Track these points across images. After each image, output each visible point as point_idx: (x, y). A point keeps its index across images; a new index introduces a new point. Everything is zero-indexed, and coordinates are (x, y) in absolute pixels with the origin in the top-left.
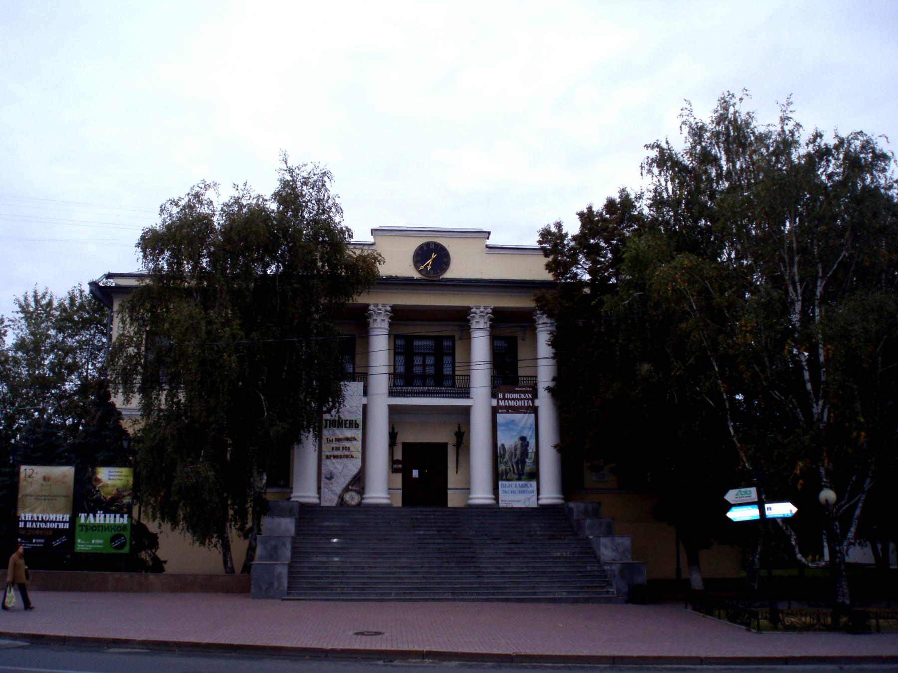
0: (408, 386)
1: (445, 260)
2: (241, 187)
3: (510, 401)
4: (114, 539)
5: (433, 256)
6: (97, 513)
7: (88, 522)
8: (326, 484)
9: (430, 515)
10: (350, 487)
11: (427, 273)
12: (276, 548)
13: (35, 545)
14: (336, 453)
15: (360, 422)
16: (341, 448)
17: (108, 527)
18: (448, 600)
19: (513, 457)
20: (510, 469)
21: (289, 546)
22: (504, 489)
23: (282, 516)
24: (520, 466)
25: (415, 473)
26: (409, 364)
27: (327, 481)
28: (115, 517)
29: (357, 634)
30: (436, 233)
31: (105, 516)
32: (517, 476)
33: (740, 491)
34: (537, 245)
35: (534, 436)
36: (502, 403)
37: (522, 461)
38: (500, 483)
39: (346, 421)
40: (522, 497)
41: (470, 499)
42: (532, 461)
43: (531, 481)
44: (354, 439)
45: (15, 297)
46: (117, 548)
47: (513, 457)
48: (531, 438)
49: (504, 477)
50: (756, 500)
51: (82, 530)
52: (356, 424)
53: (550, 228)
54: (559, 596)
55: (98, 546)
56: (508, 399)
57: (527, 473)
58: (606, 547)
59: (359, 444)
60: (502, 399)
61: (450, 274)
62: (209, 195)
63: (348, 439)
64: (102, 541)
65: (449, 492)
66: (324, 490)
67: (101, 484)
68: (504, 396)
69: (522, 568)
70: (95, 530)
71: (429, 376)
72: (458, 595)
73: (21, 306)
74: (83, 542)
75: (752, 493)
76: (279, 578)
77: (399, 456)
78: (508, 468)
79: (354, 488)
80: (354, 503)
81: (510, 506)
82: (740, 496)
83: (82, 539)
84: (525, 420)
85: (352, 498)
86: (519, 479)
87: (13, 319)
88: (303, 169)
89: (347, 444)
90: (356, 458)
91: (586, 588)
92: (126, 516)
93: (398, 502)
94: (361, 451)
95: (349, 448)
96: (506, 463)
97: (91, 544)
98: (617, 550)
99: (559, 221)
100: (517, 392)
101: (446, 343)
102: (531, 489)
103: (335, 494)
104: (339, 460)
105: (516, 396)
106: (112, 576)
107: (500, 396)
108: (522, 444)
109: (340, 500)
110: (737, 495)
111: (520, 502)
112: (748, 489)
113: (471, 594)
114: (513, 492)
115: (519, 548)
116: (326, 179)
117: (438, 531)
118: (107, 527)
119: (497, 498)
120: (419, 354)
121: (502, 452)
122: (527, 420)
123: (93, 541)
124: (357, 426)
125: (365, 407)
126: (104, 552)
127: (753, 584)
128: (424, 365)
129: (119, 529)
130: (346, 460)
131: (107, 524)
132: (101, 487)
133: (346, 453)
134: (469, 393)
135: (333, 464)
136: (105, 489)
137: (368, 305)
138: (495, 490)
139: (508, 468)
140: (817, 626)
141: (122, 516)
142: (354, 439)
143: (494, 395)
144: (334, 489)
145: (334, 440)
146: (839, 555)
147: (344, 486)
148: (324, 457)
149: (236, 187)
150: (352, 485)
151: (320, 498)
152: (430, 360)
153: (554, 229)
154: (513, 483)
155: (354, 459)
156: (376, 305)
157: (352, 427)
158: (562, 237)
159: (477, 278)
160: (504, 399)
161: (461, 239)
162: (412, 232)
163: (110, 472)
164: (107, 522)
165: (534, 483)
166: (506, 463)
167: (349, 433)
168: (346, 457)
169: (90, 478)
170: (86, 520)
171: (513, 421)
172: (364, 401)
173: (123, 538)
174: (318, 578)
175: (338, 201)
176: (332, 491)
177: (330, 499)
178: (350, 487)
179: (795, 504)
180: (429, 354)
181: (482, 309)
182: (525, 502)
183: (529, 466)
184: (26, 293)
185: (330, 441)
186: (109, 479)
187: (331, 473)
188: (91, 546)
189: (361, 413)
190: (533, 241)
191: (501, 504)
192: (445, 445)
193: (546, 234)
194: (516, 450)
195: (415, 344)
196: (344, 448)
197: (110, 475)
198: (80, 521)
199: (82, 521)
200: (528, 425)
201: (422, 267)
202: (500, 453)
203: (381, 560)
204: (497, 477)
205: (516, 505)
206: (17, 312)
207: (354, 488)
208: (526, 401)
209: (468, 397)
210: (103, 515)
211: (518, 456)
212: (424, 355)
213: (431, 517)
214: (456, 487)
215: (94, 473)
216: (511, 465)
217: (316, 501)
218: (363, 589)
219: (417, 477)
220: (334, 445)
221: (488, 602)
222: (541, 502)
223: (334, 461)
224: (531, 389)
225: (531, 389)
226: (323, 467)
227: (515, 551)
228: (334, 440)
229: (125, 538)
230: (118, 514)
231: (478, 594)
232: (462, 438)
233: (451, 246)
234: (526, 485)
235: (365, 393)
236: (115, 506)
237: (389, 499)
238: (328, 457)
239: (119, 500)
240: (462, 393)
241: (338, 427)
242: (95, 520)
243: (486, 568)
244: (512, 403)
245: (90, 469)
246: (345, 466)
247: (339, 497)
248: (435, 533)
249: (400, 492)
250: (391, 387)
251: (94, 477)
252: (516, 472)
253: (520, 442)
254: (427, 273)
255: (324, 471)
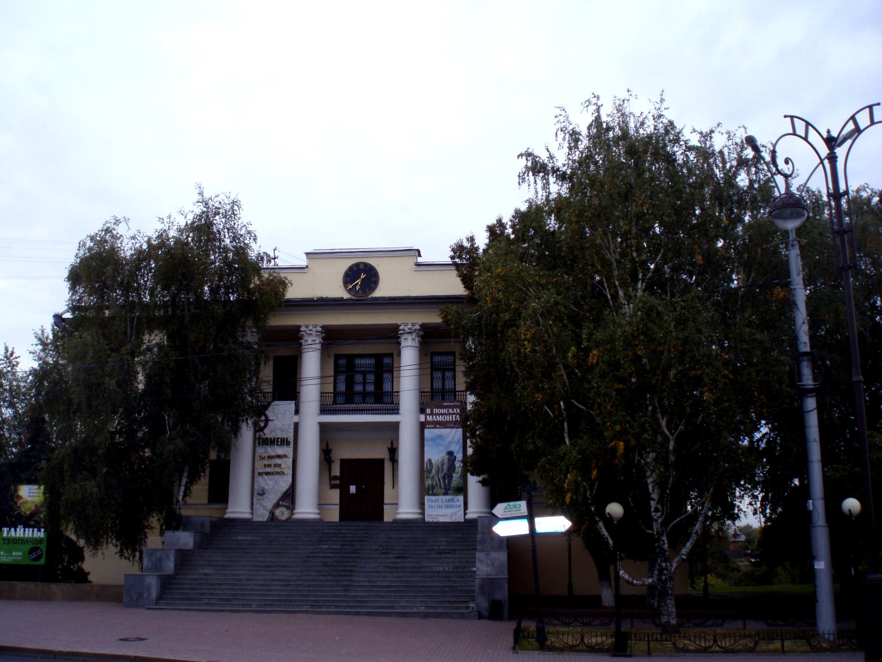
0: (380, 404)
1: (373, 279)
2: (166, 220)
3: (438, 416)
4: (32, 551)
5: (363, 276)
6: (17, 527)
7: (9, 536)
8: (258, 499)
9: (342, 530)
10: (281, 503)
11: (356, 293)
12: (160, 559)
13: (15, 558)
14: (268, 470)
15: (291, 440)
16: (273, 465)
17: (27, 540)
18: (307, 612)
19: (440, 472)
20: (436, 484)
21: (172, 559)
22: (430, 504)
23: (185, 529)
24: (447, 481)
25: (353, 489)
26: (350, 383)
27: (260, 497)
28: (33, 531)
29: (121, 640)
30: (348, 254)
31: (24, 531)
32: (443, 491)
33: (509, 505)
34: (449, 261)
35: (461, 450)
36: (430, 418)
37: (449, 476)
38: (426, 498)
39: (278, 439)
40: (449, 511)
41: (398, 514)
42: (458, 475)
43: (458, 495)
44: (286, 456)
45: (33, 332)
46: (33, 560)
47: (440, 472)
48: (458, 452)
49: (430, 492)
50: (526, 514)
51: (4, 543)
52: (287, 441)
53: (462, 243)
54: (418, 611)
55: (18, 558)
56: (436, 415)
57: (454, 487)
58: (481, 561)
59: (289, 461)
60: (429, 415)
61: (379, 293)
62: (121, 230)
63: (279, 457)
64: (20, 554)
65: (385, 507)
66: (256, 506)
67: (22, 501)
68: (432, 411)
69: (393, 582)
70: (15, 543)
71: (370, 393)
72: (316, 607)
73: (40, 339)
74: (5, 554)
75: (522, 506)
76: (149, 588)
77: (336, 471)
78: (434, 483)
79: (284, 504)
80: (283, 518)
81: (435, 520)
82: (509, 510)
83: (4, 552)
84: (452, 434)
85: (282, 514)
86: (446, 494)
87: (33, 351)
88: (216, 199)
89: (278, 461)
90: (287, 474)
91: (448, 603)
92: (42, 530)
93: (334, 515)
94: (291, 468)
95: (280, 465)
96: (433, 478)
97: (12, 556)
98: (493, 564)
99: (471, 235)
100: (446, 407)
101: (387, 361)
102: (457, 503)
103: (266, 510)
104: (271, 477)
105: (445, 411)
106: (19, 585)
107: (428, 411)
108: (449, 458)
109: (271, 515)
110: (506, 508)
111: (446, 517)
112: (518, 503)
113: (329, 607)
114: (440, 507)
115: (404, 562)
116: (236, 208)
117: (342, 545)
118: (25, 540)
119: (423, 513)
120: (360, 372)
121: (429, 467)
122: (455, 434)
123: (14, 554)
124: (288, 443)
125: (296, 426)
126: (24, 563)
127: (653, 601)
128: (364, 383)
129: (37, 542)
130: (277, 476)
131: (19, 537)
132: (21, 503)
133: (278, 470)
134: (398, 410)
135: (265, 480)
136: (25, 505)
137: (300, 327)
138: (422, 505)
139: (434, 483)
140: (580, 647)
141: (39, 530)
142: (286, 456)
143: (422, 411)
144: (265, 504)
145: (266, 458)
146: (665, 572)
147: (275, 501)
148: (256, 474)
149: (161, 220)
150: (283, 501)
151: (252, 514)
152: (371, 378)
153: (466, 244)
154: (440, 497)
155: (285, 476)
156: (307, 327)
157: (284, 445)
158: (474, 249)
159: (391, 296)
160: (432, 414)
161: (403, 258)
162: (342, 254)
163: (30, 489)
164: (26, 535)
165: (461, 498)
166: (433, 478)
167: (280, 450)
168: (278, 473)
169: (12, 495)
170: (8, 534)
171: (440, 436)
172: (296, 419)
173: (39, 550)
174: (193, 589)
175: (250, 228)
176: (263, 506)
177: (262, 515)
178: (281, 503)
179: (570, 518)
180: (370, 372)
181: (410, 326)
182: (451, 517)
183: (456, 480)
184: (42, 327)
185: (263, 459)
186: (29, 496)
187: (263, 490)
188: (12, 558)
189: (292, 431)
190: (445, 256)
191: (428, 519)
192: (381, 462)
193: (459, 250)
194: (443, 465)
195: (385, 362)
196: (275, 465)
197: (30, 493)
198: (3, 534)
199: (5, 534)
200: (456, 440)
201: (350, 287)
202: (427, 468)
203: (264, 573)
204: (424, 491)
205: (441, 520)
206: (37, 345)
207: (284, 504)
208: (454, 416)
209: (398, 413)
210: (22, 529)
211: (445, 470)
212: (365, 373)
213: (343, 531)
214: (392, 502)
215: (16, 490)
216: (437, 480)
217: (248, 516)
218: (228, 600)
219: (355, 492)
220: (266, 462)
221: (339, 614)
222: (468, 517)
223: (266, 477)
224: (459, 404)
225: (459, 404)
226: (256, 484)
227: (400, 565)
228: (266, 458)
229: (41, 551)
230: (36, 528)
231: (336, 606)
232: (393, 452)
233: (290, 276)
234: (453, 500)
235: (297, 412)
236: (33, 521)
237: (319, 514)
238: (260, 474)
239: (37, 516)
240: (392, 410)
241: (270, 445)
242: (16, 534)
243: (359, 581)
244: (440, 418)
245: (13, 487)
246: (276, 482)
247: (270, 512)
248: (339, 547)
249: (338, 507)
250: (322, 405)
251: (15, 496)
252: (442, 486)
253: (448, 457)
254: (356, 293)
255: (256, 488)
